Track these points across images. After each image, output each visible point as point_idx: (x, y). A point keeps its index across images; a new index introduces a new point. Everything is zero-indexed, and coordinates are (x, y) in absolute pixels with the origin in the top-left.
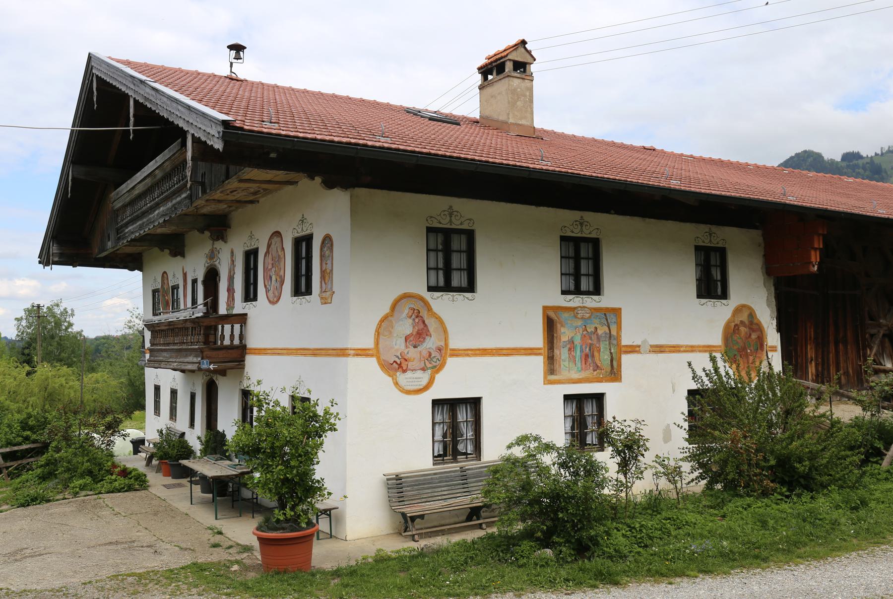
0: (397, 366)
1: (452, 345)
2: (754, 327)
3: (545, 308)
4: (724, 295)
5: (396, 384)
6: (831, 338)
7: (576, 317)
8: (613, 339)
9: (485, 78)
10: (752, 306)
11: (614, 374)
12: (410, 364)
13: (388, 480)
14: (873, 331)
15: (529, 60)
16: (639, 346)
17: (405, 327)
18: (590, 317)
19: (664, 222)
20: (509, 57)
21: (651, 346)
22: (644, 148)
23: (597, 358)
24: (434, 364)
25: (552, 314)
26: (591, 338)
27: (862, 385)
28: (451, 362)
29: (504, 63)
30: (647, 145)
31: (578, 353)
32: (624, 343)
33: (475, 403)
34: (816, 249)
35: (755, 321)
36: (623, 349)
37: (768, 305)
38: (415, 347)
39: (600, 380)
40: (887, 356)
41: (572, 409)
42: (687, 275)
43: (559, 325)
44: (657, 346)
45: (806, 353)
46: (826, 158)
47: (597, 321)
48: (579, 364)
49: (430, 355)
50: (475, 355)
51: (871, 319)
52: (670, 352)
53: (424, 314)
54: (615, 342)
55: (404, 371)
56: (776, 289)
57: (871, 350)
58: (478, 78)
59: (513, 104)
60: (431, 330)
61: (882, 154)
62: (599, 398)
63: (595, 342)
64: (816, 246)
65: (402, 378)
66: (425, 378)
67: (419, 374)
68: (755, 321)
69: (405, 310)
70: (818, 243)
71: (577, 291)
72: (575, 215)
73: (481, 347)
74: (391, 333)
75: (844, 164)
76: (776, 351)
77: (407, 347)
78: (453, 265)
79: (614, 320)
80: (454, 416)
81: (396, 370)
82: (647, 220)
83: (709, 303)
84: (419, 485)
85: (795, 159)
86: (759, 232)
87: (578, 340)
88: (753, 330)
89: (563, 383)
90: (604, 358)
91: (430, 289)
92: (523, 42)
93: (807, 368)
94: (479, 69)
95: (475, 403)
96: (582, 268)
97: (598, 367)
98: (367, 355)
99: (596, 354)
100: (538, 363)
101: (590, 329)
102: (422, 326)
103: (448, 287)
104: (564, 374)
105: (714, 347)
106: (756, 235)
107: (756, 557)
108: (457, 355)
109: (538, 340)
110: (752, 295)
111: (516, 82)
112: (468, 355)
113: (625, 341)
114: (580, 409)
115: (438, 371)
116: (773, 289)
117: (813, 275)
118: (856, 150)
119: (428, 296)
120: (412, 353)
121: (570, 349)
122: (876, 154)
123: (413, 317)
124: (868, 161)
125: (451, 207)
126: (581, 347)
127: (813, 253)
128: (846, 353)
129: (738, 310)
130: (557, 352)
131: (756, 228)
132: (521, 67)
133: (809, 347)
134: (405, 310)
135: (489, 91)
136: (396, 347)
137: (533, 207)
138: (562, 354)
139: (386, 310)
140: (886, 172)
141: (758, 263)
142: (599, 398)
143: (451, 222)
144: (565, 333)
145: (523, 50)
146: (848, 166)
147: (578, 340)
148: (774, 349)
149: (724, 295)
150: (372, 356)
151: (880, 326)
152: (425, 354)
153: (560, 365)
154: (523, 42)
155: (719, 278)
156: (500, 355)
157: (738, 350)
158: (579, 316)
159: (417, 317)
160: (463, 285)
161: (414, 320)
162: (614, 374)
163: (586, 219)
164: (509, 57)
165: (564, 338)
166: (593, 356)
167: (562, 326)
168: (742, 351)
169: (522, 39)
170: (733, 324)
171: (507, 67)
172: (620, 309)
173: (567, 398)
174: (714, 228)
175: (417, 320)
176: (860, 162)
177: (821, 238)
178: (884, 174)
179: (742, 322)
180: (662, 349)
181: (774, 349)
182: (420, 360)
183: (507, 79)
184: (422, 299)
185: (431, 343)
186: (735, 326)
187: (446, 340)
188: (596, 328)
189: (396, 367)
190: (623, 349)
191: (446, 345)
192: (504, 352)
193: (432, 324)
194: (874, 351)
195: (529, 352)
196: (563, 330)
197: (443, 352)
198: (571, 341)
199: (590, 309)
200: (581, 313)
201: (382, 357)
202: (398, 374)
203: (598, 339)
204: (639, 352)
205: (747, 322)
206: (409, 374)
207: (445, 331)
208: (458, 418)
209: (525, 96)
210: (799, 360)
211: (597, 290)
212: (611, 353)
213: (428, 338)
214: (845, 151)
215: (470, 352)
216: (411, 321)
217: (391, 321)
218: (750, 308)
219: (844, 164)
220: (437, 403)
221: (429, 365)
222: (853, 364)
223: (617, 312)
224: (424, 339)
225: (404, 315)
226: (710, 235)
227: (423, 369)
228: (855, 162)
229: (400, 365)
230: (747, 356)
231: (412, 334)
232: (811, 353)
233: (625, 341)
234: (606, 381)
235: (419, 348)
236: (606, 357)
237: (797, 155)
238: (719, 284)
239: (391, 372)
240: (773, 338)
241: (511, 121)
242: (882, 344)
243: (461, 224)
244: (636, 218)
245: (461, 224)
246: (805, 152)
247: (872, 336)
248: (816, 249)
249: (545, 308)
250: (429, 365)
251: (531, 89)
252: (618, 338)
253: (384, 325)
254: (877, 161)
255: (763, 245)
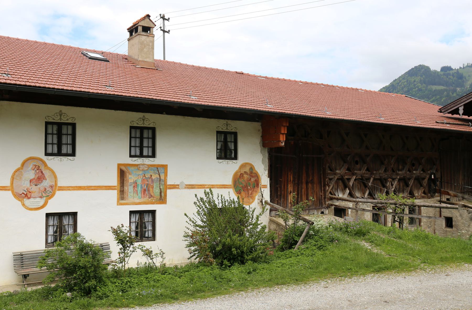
0: (24, 196)
1: (60, 184)
2: (253, 175)
3: (119, 165)
4: (236, 158)
5: (24, 205)
6: (304, 181)
7: (138, 169)
8: (162, 181)
9: (131, 35)
10: (253, 164)
11: (162, 199)
12: (32, 195)
13: (14, 255)
14: (331, 177)
15: (151, 25)
16: (178, 185)
17: (31, 174)
18: (147, 170)
19: (197, 118)
20: (139, 24)
21: (186, 185)
22: (237, 73)
23: (151, 192)
24: (48, 194)
25: (123, 168)
26: (148, 181)
27: (322, 206)
28: (58, 193)
29: (137, 27)
30: (239, 71)
31: (139, 189)
32: (168, 183)
33: (74, 214)
34: (283, 134)
35: (254, 172)
36: (168, 187)
37: (263, 163)
38: (36, 185)
39: (153, 203)
40: (340, 190)
41: (135, 218)
42: (211, 147)
43: (127, 174)
44: (190, 185)
45: (287, 189)
46: (432, 69)
47: (152, 172)
48: (140, 195)
49: (45, 189)
50: (74, 190)
51: (331, 170)
52: (198, 188)
53: (42, 168)
54: (163, 183)
55: (29, 198)
56: (269, 154)
57: (329, 186)
58: (128, 34)
59: (141, 50)
60: (47, 176)
61: (464, 68)
62: (153, 213)
63: (150, 183)
64: (282, 132)
65: (27, 202)
66: (42, 202)
67: (38, 199)
68: (254, 172)
69: (31, 165)
70: (284, 130)
71: (141, 155)
72: (140, 115)
73: (78, 185)
74: (21, 178)
75: (442, 73)
76: (266, 187)
77: (31, 185)
78: (61, 140)
79: (163, 171)
80: (142, 134)
81: (24, 198)
82: (186, 117)
83: (225, 162)
84: (33, 258)
85: (415, 70)
86: (259, 124)
87: (139, 182)
88: (252, 177)
89: (129, 205)
90: (156, 191)
91: (47, 154)
92: (148, 16)
93: (287, 196)
94: (128, 29)
95: (74, 214)
96: (143, 142)
97: (152, 196)
98: (6, 190)
99: (151, 189)
100: (114, 194)
101: (148, 176)
102: (41, 174)
103: (59, 154)
104: (130, 200)
105: (227, 185)
106: (257, 125)
107: (172, 298)
108: (62, 190)
109: (114, 180)
110: (253, 157)
111: (143, 38)
112: (69, 190)
113: (169, 183)
114: (141, 218)
115: (50, 198)
116: (267, 155)
117: (281, 148)
118: (449, 65)
119: (45, 158)
120: (34, 188)
121: (134, 187)
122: (460, 68)
123: (35, 169)
124: (456, 71)
125: (61, 111)
126: (141, 185)
127: (281, 136)
128: (313, 189)
129: (243, 166)
130: (126, 188)
131: (258, 121)
132: (146, 29)
133: (289, 185)
134: (31, 165)
135: (131, 41)
136: (24, 186)
137: (113, 111)
138: (129, 189)
139: (19, 165)
140: (465, 78)
141: (257, 141)
142: (153, 213)
143: (61, 119)
144: (131, 178)
145: (148, 20)
146: (444, 74)
147: (139, 182)
148: (265, 186)
149: (236, 158)
150: (9, 190)
151: (335, 174)
152: (42, 189)
153: (128, 195)
154: (148, 16)
155: (233, 148)
156: (89, 190)
157: (242, 187)
158: (141, 169)
159: (38, 169)
160: (69, 152)
161: (36, 171)
162: (162, 199)
163: (146, 117)
164: (139, 24)
165: (131, 181)
166: (149, 190)
167: (130, 174)
168: (245, 188)
169: (147, 14)
170: (240, 173)
171: (141, 29)
172: (167, 165)
173: (131, 213)
174: (229, 122)
175: (37, 171)
176: (451, 72)
177: (286, 128)
178: (464, 79)
179: (245, 172)
180: (193, 187)
181: (265, 186)
182: (39, 193)
183: (138, 36)
184: (41, 160)
185: (46, 183)
186: (241, 174)
187: (56, 182)
188: (151, 176)
189: (24, 196)
190: (168, 187)
191: (56, 184)
192: (92, 188)
193: (47, 173)
194: (331, 187)
195: (108, 188)
196: (130, 176)
197: (54, 188)
198: (135, 183)
199: (148, 165)
200: (142, 168)
201: (15, 191)
202: (25, 199)
203: (153, 181)
204: (178, 188)
205: (248, 172)
206: (32, 200)
207: (55, 177)
208: (61, 224)
209: (149, 45)
210: (283, 192)
211: (154, 156)
212: (160, 189)
213: (44, 181)
214: (443, 66)
215: (70, 188)
216: (34, 172)
217: (21, 172)
218: (250, 164)
219: (442, 73)
220: (48, 215)
221: (44, 195)
222: (317, 194)
223: (165, 167)
224: (42, 181)
225: (30, 168)
226: (227, 125)
227: (41, 197)
228: (448, 72)
229: (26, 195)
230: (248, 190)
231: (34, 179)
232: (290, 188)
233: (169, 183)
234: (157, 204)
235: (38, 186)
236: (157, 191)
237: (415, 67)
238: (233, 151)
239: (21, 199)
240: (265, 180)
241: (140, 59)
242: (337, 183)
243: (67, 120)
244: (179, 116)
245: (67, 120)
246: (420, 65)
247: (331, 179)
248: (283, 134)
249: (119, 165)
250: (44, 195)
251: (153, 42)
252: (165, 180)
253: (17, 174)
254: (460, 72)
255: (261, 130)
